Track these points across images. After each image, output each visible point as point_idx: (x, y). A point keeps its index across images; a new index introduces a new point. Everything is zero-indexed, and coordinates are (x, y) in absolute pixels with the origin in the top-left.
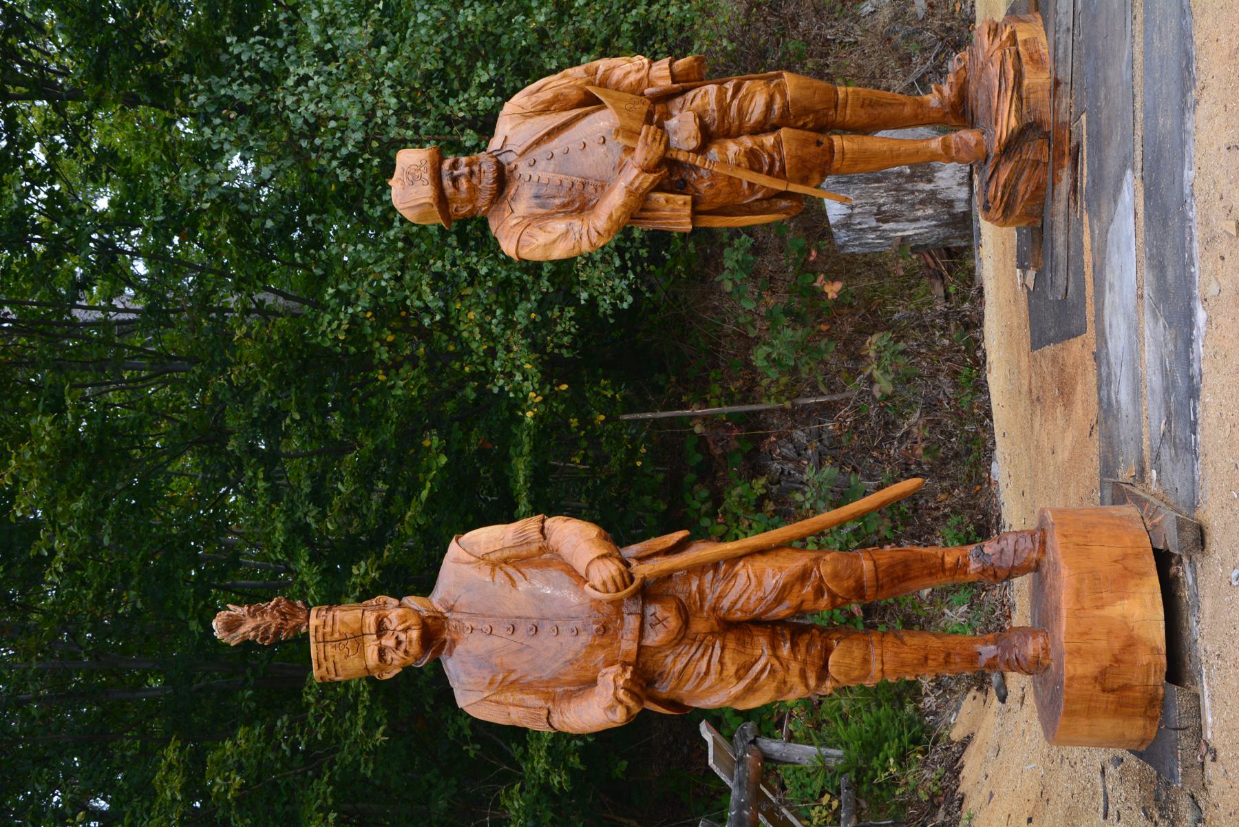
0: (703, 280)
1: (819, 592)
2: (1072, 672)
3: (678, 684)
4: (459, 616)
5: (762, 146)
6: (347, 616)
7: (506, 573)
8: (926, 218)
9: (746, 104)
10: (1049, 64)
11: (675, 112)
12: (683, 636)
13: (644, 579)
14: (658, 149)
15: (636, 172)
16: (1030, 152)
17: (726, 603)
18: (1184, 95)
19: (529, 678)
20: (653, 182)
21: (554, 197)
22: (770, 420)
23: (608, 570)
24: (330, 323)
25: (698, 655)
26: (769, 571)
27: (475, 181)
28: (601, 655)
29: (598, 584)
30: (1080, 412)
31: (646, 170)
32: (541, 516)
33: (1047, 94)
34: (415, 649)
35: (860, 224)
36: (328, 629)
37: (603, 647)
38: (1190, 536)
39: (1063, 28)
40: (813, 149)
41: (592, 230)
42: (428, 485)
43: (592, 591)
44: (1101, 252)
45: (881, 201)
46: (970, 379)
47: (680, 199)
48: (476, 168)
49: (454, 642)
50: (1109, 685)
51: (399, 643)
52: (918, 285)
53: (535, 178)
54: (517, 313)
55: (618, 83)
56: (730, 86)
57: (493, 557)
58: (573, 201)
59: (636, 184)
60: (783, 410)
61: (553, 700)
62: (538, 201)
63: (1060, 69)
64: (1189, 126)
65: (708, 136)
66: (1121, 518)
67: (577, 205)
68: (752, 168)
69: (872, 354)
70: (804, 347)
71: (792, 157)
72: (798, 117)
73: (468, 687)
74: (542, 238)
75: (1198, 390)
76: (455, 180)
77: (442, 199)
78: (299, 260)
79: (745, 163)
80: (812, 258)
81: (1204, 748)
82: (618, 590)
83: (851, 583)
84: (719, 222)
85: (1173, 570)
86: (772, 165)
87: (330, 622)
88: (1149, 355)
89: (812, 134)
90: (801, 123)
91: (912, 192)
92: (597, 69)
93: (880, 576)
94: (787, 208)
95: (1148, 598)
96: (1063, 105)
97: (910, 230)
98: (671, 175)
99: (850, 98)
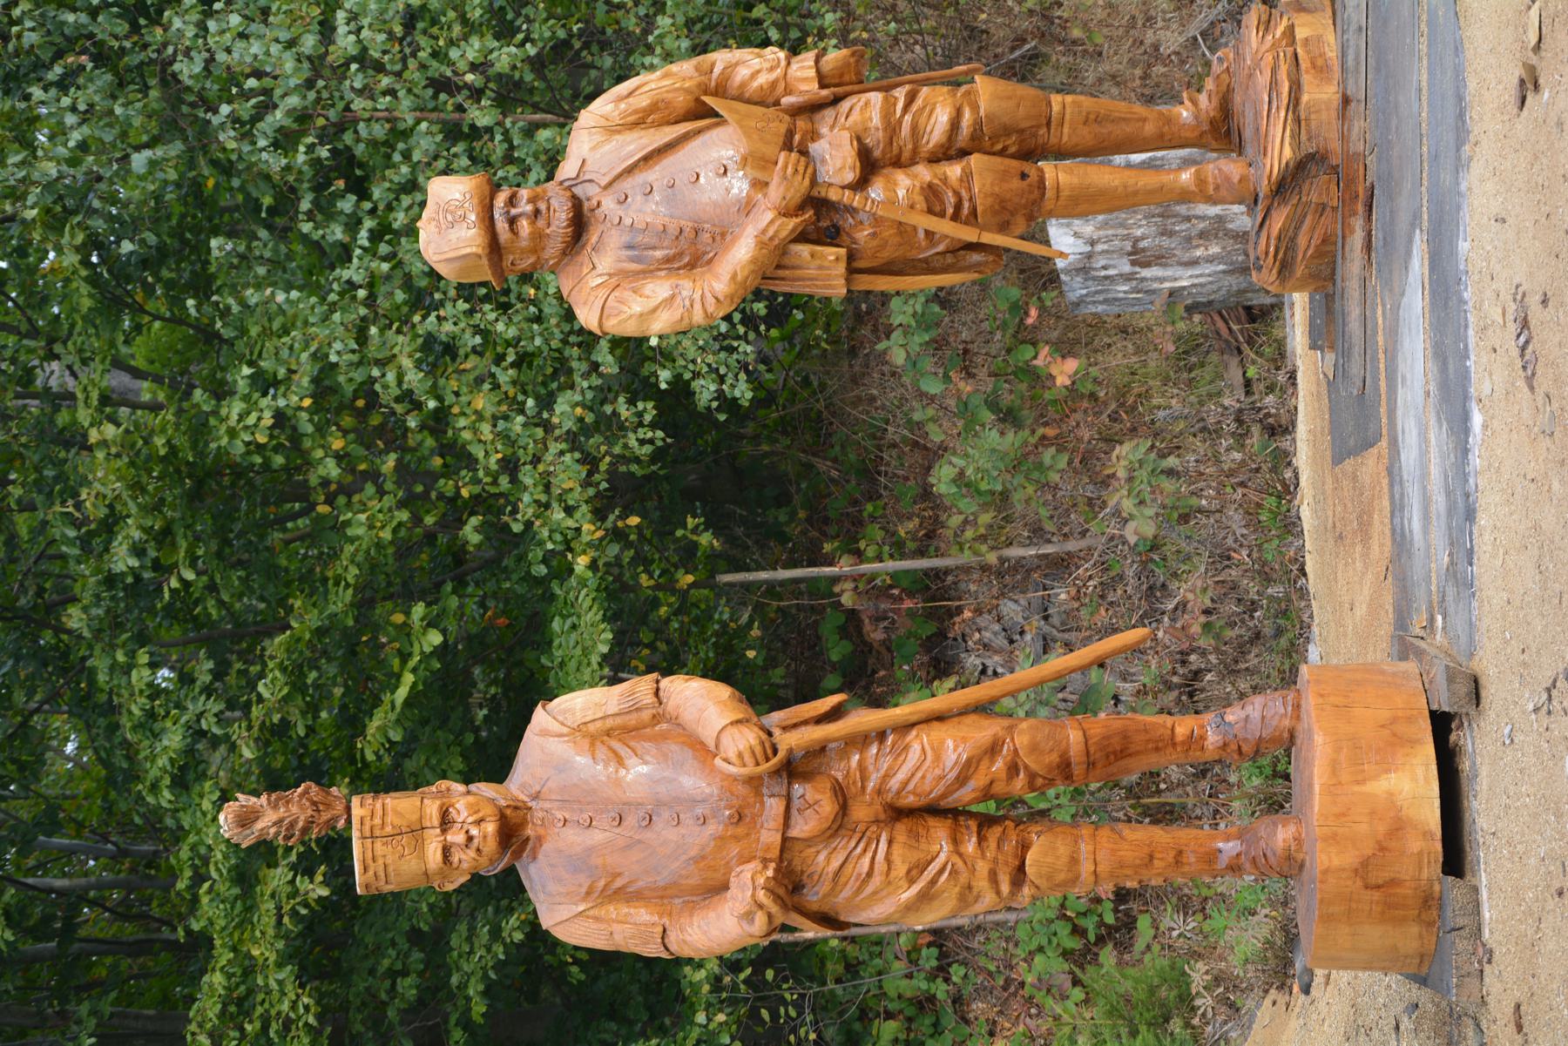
0: (853, 352)
1: (1013, 769)
2: (1326, 863)
3: (833, 889)
4: (547, 805)
5: (945, 180)
6: (400, 806)
7: (610, 748)
8: (1210, 260)
9: (922, 120)
10: (1337, 74)
11: (824, 130)
12: (840, 825)
13: (790, 751)
14: (801, 186)
15: (770, 215)
16: (1317, 190)
17: (894, 783)
18: (1458, 150)
19: (641, 884)
20: (793, 230)
21: (654, 248)
22: (962, 586)
23: (744, 739)
24: (241, 418)
25: (859, 850)
26: (950, 743)
27: (541, 223)
28: (734, 850)
29: (732, 755)
30: (1376, 547)
31: (786, 213)
32: (655, 675)
33: (1334, 114)
34: (491, 846)
35: (1105, 268)
36: (377, 821)
37: (736, 838)
38: (1463, 688)
39: (1353, 27)
40: (1016, 183)
41: (709, 296)
42: (409, 678)
43: (725, 765)
44: (1393, 332)
45: (1139, 233)
46: (1275, 514)
47: (831, 253)
48: (543, 206)
49: (540, 839)
50: (1373, 881)
51: (470, 839)
52: (1202, 365)
53: (628, 221)
54: (558, 409)
55: (743, 85)
56: (900, 94)
57: (591, 727)
58: (681, 254)
59: (771, 233)
60: (985, 568)
61: (670, 915)
62: (630, 253)
63: (1351, 82)
64: (1463, 187)
65: (869, 166)
66: (1394, 674)
67: (686, 260)
68: (930, 211)
69: (1122, 474)
70: (1018, 463)
71: (986, 196)
72: (994, 138)
73: (558, 899)
74: (637, 306)
75: (1474, 511)
76: (512, 221)
77: (495, 248)
78: (193, 311)
79: (921, 204)
80: (1030, 321)
81: (1480, 950)
82: (758, 764)
83: (1054, 758)
84: (883, 284)
85: (1453, 737)
86: (958, 206)
87: (379, 812)
88: (1435, 471)
89: (1015, 163)
90: (999, 147)
91: (1188, 219)
92: (713, 65)
93: (1092, 750)
94: (979, 264)
95: (1420, 771)
96: (1356, 130)
97: (1184, 279)
98: (818, 220)
99: (1068, 111)
